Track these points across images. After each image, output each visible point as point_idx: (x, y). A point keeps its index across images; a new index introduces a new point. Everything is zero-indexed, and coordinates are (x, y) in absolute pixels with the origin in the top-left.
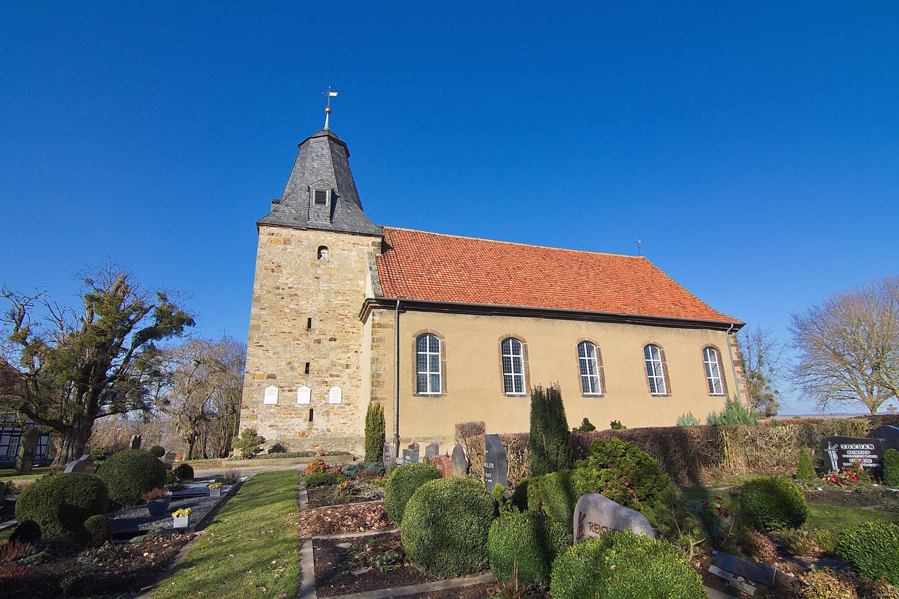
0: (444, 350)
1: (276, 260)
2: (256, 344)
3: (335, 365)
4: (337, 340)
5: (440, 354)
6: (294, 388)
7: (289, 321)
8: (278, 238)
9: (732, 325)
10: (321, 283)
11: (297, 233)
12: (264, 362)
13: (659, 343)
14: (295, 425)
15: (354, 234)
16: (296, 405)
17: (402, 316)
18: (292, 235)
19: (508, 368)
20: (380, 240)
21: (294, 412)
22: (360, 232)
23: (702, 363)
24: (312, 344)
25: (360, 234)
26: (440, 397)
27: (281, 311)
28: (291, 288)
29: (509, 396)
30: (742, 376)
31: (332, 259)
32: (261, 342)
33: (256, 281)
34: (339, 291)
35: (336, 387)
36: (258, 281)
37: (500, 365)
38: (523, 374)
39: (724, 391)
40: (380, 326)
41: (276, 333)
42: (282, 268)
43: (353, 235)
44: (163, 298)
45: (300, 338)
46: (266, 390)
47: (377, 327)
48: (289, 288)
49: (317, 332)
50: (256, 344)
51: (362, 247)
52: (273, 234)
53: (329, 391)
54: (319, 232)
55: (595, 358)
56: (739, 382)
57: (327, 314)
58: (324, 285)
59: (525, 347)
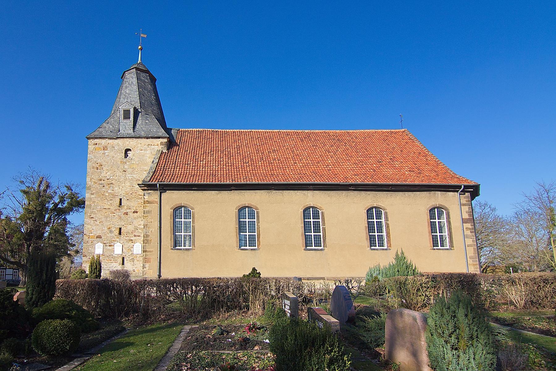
0: (258, 217)
1: (99, 161)
2: (89, 217)
3: (137, 229)
4: (138, 213)
5: (320, 220)
6: (112, 244)
7: (108, 201)
8: (100, 146)
9: (463, 187)
10: (127, 174)
11: (111, 142)
12: (94, 228)
13: (382, 205)
14: (113, 267)
15: (148, 138)
16: (114, 255)
17: (163, 195)
18: (108, 144)
19: (372, 229)
20: (166, 140)
21: (113, 259)
22: (152, 136)
23: (426, 221)
24: (123, 216)
25: (152, 138)
26: (190, 250)
27: (103, 195)
28: (108, 179)
29: (374, 249)
30: (471, 232)
31: (134, 157)
32: (92, 215)
33: (87, 176)
34: (139, 179)
35: (138, 243)
36: (89, 176)
37: (236, 227)
38: (384, 234)
39: (449, 246)
40: (149, 202)
41: (100, 209)
42: (103, 167)
43: (147, 139)
44: (69, 188)
45: (115, 212)
46: (96, 245)
47: (146, 203)
48: (107, 179)
49: (125, 207)
50: (89, 217)
51: (154, 147)
52: (97, 144)
53: (134, 246)
54: (125, 139)
55: (444, 220)
56: (467, 238)
57: (131, 195)
58: (129, 176)
59: (386, 214)
